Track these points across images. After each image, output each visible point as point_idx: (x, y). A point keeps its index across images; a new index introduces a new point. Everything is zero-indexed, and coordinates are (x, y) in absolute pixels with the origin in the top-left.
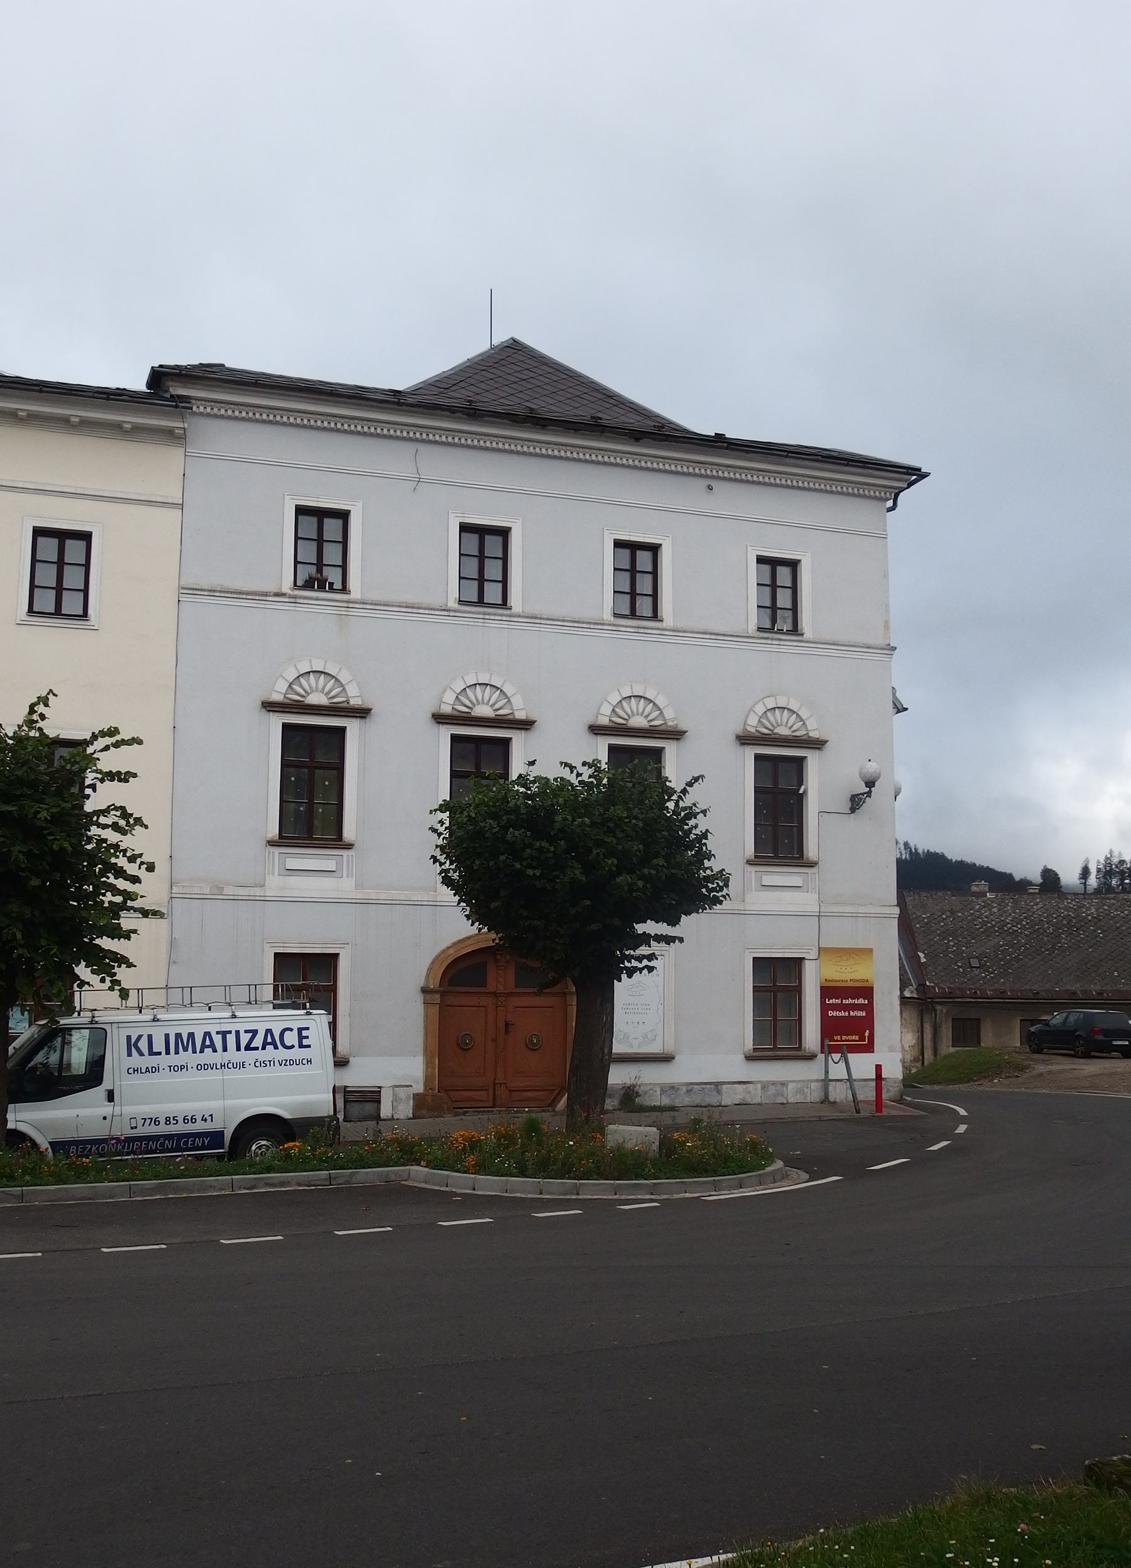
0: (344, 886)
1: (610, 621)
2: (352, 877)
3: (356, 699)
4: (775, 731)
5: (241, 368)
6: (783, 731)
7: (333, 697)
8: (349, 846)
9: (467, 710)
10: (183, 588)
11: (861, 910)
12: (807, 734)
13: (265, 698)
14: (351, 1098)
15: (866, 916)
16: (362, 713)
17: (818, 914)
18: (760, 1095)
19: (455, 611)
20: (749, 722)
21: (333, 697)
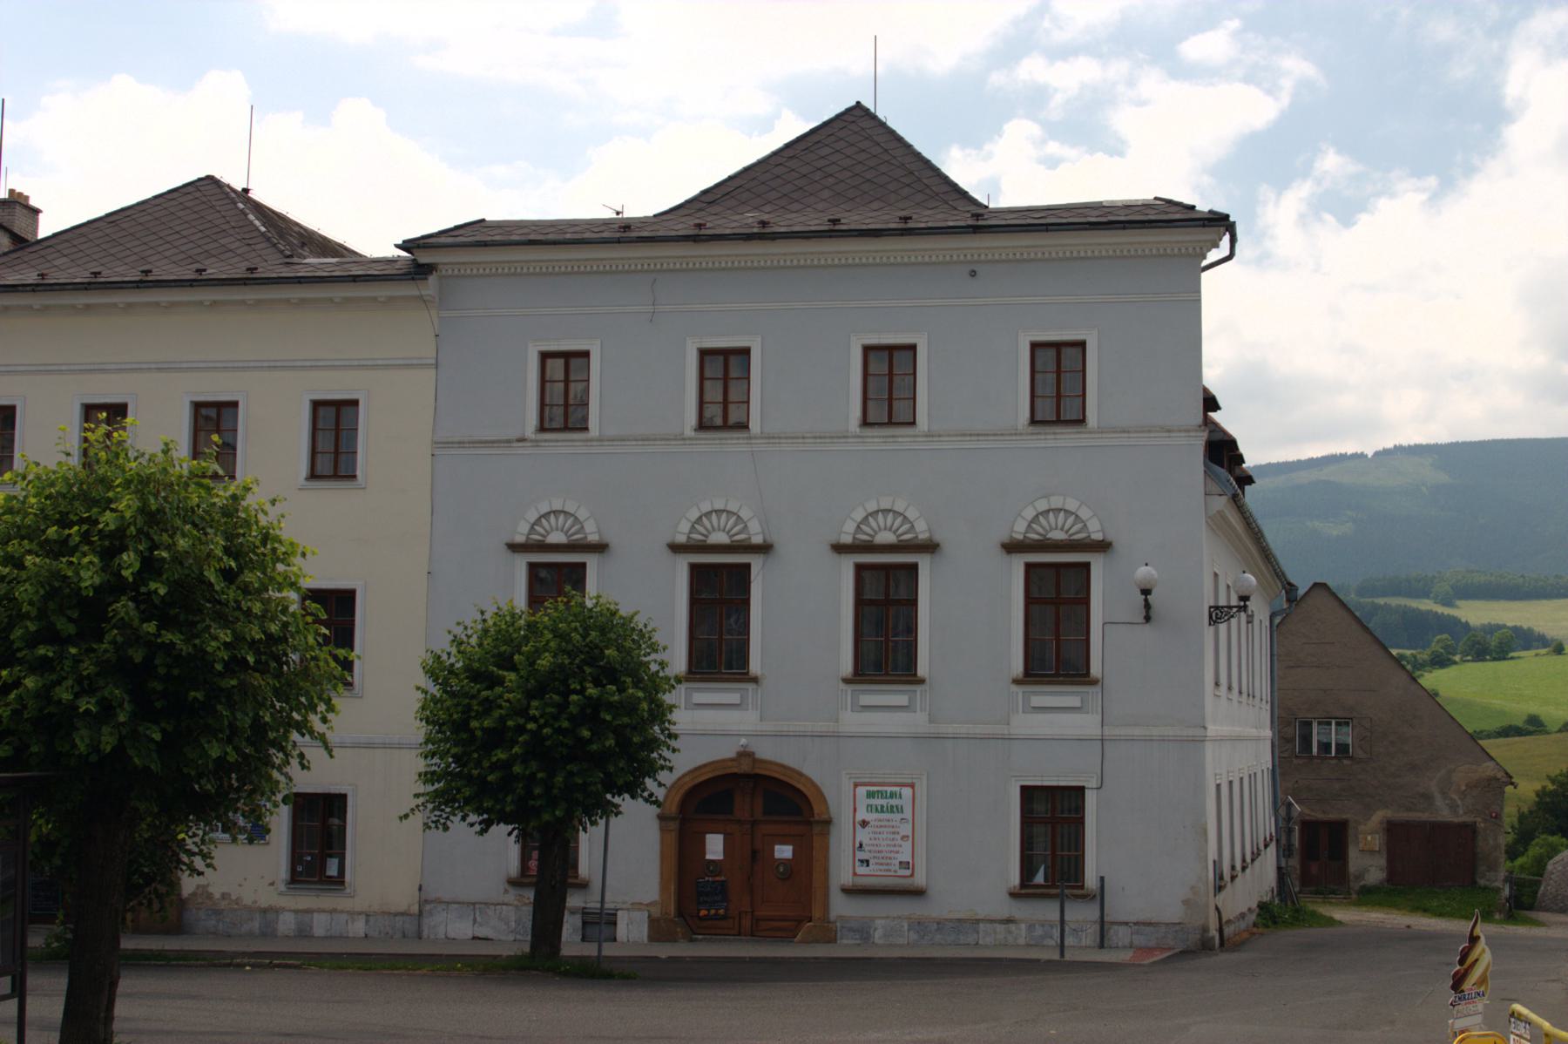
0: (917, 721)
1: (855, 432)
2: (925, 711)
3: (593, 535)
4: (1049, 536)
5: (1046, 204)
6: (1058, 535)
7: (572, 535)
8: (922, 681)
9: (703, 538)
10: (435, 443)
11: (1155, 732)
12: (1089, 536)
13: (508, 540)
14: (589, 919)
15: (1162, 739)
16: (930, 547)
17: (1100, 738)
18: (1024, 936)
19: (690, 439)
20: (1015, 529)
21: (572, 535)
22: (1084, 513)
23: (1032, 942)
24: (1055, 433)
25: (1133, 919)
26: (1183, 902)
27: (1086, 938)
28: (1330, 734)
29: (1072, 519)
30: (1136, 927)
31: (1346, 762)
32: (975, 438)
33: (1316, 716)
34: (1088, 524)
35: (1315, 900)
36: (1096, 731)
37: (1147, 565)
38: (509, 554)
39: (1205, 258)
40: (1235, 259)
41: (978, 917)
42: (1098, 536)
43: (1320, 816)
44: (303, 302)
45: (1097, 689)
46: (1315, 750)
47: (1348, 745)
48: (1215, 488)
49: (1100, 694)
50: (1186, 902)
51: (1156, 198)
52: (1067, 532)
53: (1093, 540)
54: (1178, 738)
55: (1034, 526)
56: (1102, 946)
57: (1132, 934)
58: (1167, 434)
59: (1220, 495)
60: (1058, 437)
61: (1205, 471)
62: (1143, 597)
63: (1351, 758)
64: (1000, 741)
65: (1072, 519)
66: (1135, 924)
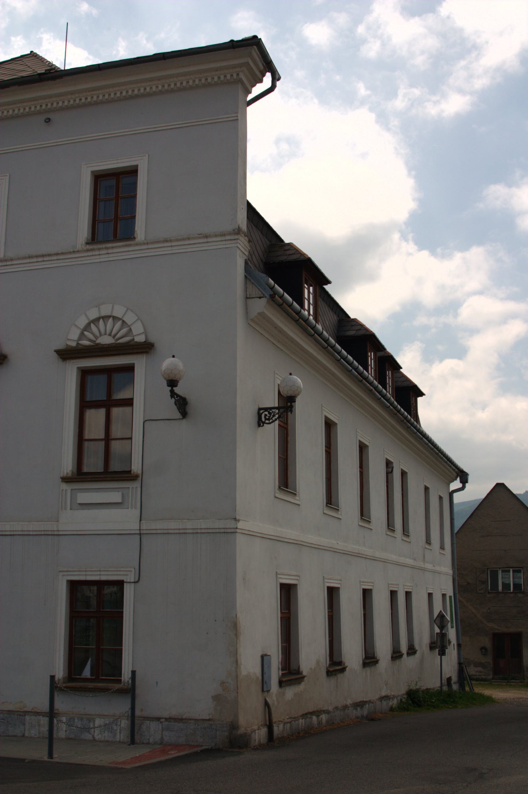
4: (98, 341)
6: (106, 340)
11: (189, 525)
15: (196, 533)
17: (138, 532)
22: (130, 318)
23: (72, 736)
24: (107, 248)
25: (166, 715)
26: (212, 697)
27: (120, 732)
28: (510, 578)
29: (119, 323)
30: (167, 723)
31: (520, 595)
32: (40, 259)
33: (500, 567)
34: (133, 328)
35: (501, 683)
36: (134, 526)
37: (174, 357)
39: (250, 92)
40: (276, 90)
41: (26, 709)
42: (140, 339)
43: (504, 630)
45: (136, 484)
46: (500, 588)
47: (521, 584)
48: (254, 291)
49: (139, 489)
50: (216, 698)
52: (114, 337)
53: (137, 342)
54: (211, 531)
56: (133, 742)
57: (163, 730)
58: (205, 240)
59: (260, 298)
60: (110, 251)
61: (246, 277)
62: (170, 388)
63: (523, 593)
64: (50, 537)
65: (119, 323)
66: (166, 719)
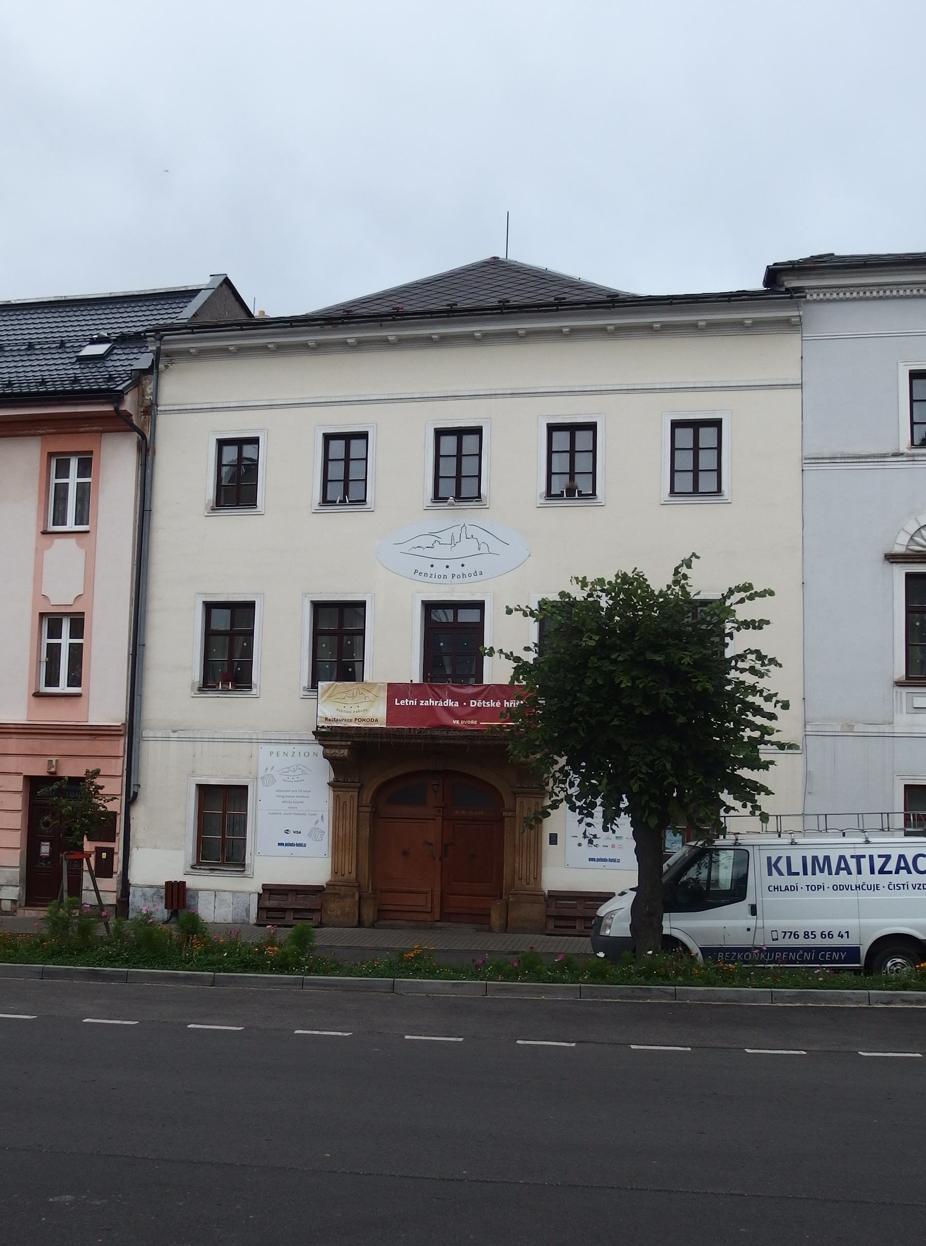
38: (887, 566)
44: (445, 341)
51: (775, 264)
55: (916, 538)
